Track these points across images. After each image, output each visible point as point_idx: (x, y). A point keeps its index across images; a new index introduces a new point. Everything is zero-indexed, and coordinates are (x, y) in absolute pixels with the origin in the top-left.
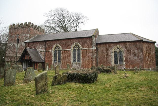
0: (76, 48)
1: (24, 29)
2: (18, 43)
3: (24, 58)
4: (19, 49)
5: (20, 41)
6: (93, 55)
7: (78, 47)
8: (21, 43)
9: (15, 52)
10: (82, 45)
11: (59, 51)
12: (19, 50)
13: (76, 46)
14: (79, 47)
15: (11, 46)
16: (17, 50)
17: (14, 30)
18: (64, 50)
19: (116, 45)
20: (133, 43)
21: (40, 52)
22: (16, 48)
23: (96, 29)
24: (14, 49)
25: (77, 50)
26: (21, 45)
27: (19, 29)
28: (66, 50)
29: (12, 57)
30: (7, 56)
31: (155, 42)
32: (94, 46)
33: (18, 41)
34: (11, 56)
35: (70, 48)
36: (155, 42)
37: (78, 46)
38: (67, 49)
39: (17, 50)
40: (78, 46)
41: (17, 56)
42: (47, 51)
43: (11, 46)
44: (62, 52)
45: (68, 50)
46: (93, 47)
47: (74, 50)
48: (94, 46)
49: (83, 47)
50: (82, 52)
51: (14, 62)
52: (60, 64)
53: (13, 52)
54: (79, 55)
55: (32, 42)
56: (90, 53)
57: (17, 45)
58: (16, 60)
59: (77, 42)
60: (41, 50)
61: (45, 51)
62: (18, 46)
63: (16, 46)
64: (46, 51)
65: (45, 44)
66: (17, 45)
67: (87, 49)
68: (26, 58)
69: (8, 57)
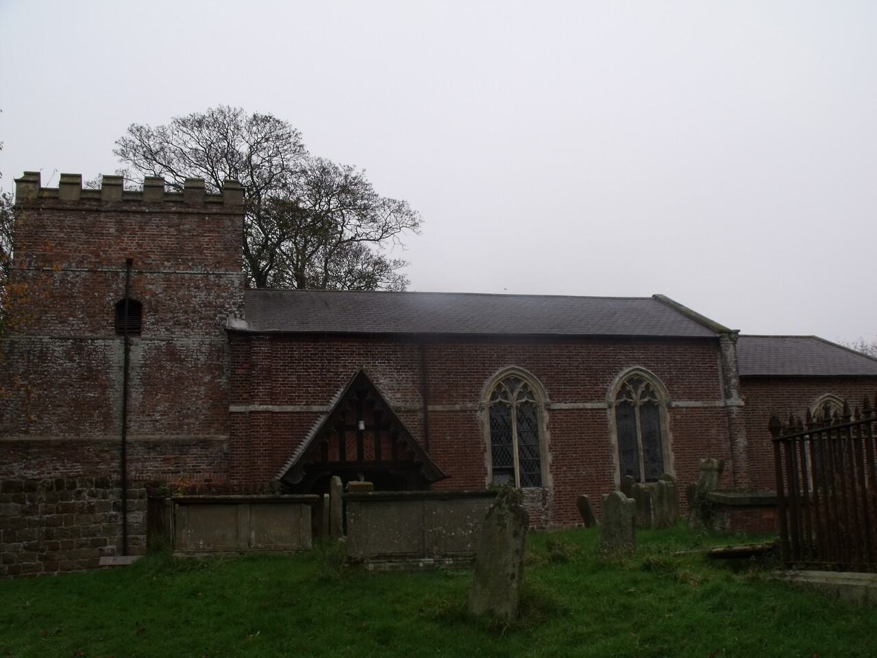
0: (636, 398)
1: (189, 224)
2: (136, 329)
5: (148, 320)
6: (732, 440)
7: (520, 395)
10: (670, 383)
11: (528, 415)
13: (505, 388)
14: (648, 391)
16: (126, 394)
18: (563, 406)
19: (820, 393)
22: (116, 376)
24: (91, 376)
25: (637, 410)
28: (581, 405)
31: (739, 331)
32: (734, 392)
33: (129, 316)
34: (57, 435)
35: (601, 396)
36: (739, 331)
37: (642, 387)
38: (586, 400)
39: (126, 394)
40: (642, 387)
41: (128, 438)
42: (438, 408)
43: (58, 349)
45: (589, 405)
46: (728, 395)
47: (624, 410)
48: (734, 392)
49: (675, 395)
50: (675, 420)
51: (92, 495)
52: (545, 494)
54: (653, 439)
56: (714, 431)
57: (127, 351)
58: (124, 472)
59: (638, 361)
61: (425, 410)
62: (137, 355)
64: (430, 408)
66: (127, 351)
67: (699, 404)
68: (343, 455)
69: (27, 445)
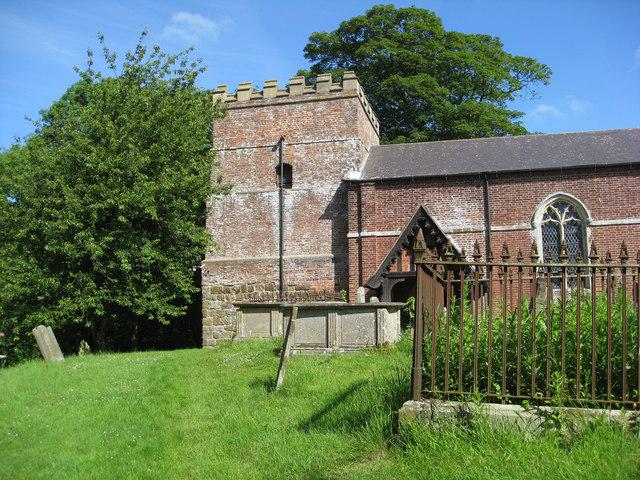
1: (321, 107)
2: (289, 184)
3: (400, 262)
4: (296, 218)
5: (296, 177)
8: (306, 186)
9: (268, 235)
12: (296, 227)
15: (240, 201)
17: (245, 114)
18: (604, 222)
20: (394, 193)
21: (457, 232)
22: (276, 217)
23: (337, 28)
24: (262, 217)
26: (311, 198)
27: (284, 109)
28: (619, 221)
29: (248, 266)
30: (213, 259)
33: (285, 174)
34: (242, 256)
38: (623, 216)
44: (594, 234)
49: (597, 214)
53: (253, 235)
55: (397, 179)
60: (462, 224)
62: (289, 201)
63: (275, 202)
65: (481, 189)
69: (224, 263)
